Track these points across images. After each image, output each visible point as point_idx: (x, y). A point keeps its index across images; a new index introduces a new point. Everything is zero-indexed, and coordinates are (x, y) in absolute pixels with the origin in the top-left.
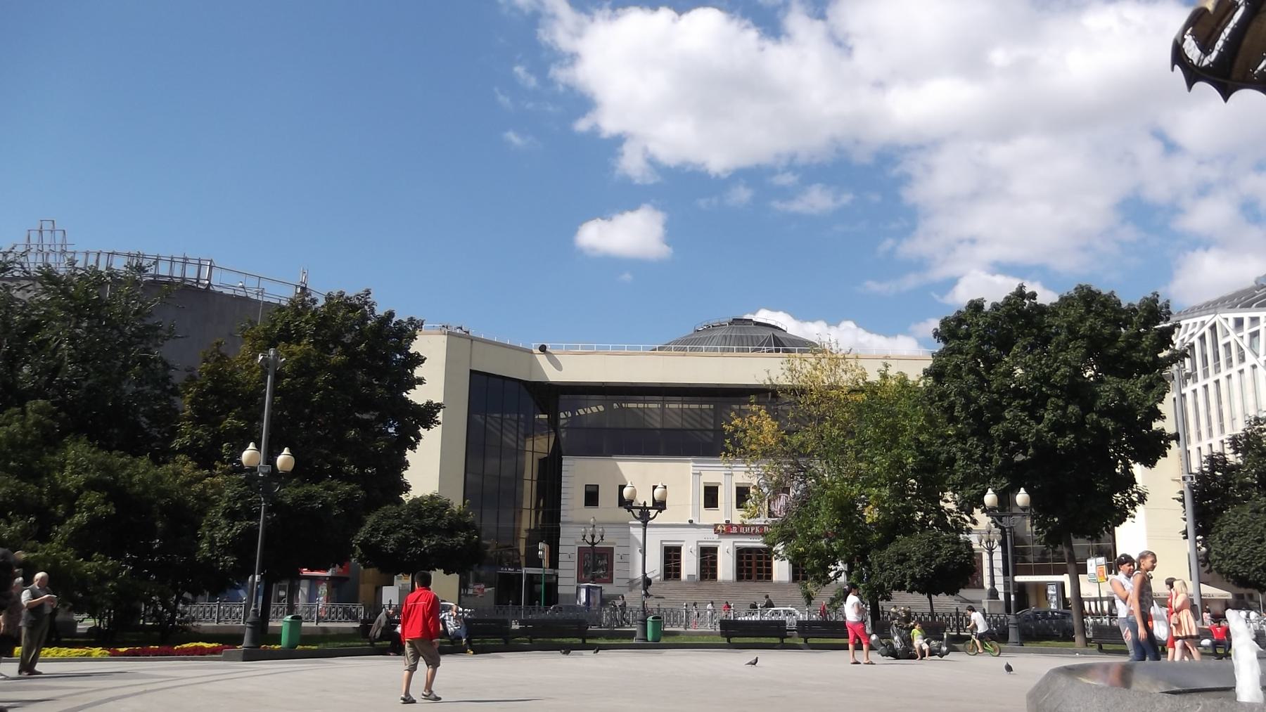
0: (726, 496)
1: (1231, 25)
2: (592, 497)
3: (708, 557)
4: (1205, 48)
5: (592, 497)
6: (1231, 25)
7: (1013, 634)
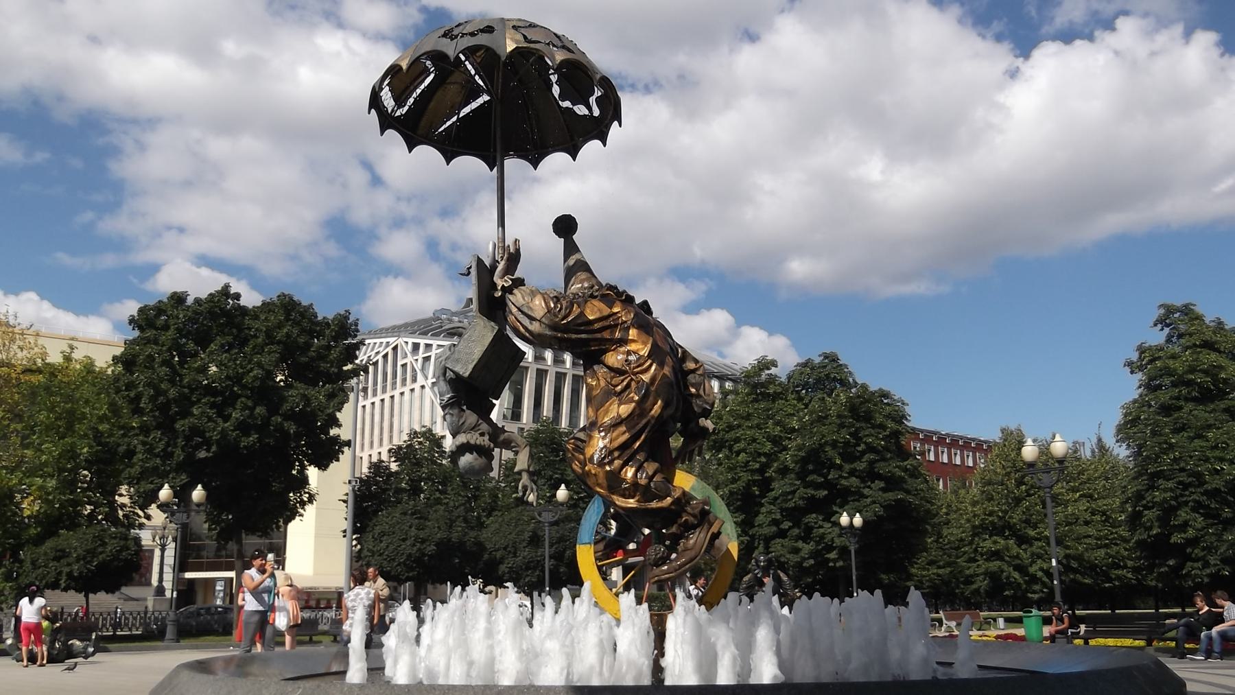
1: (422, 87)
4: (400, 102)
6: (422, 87)
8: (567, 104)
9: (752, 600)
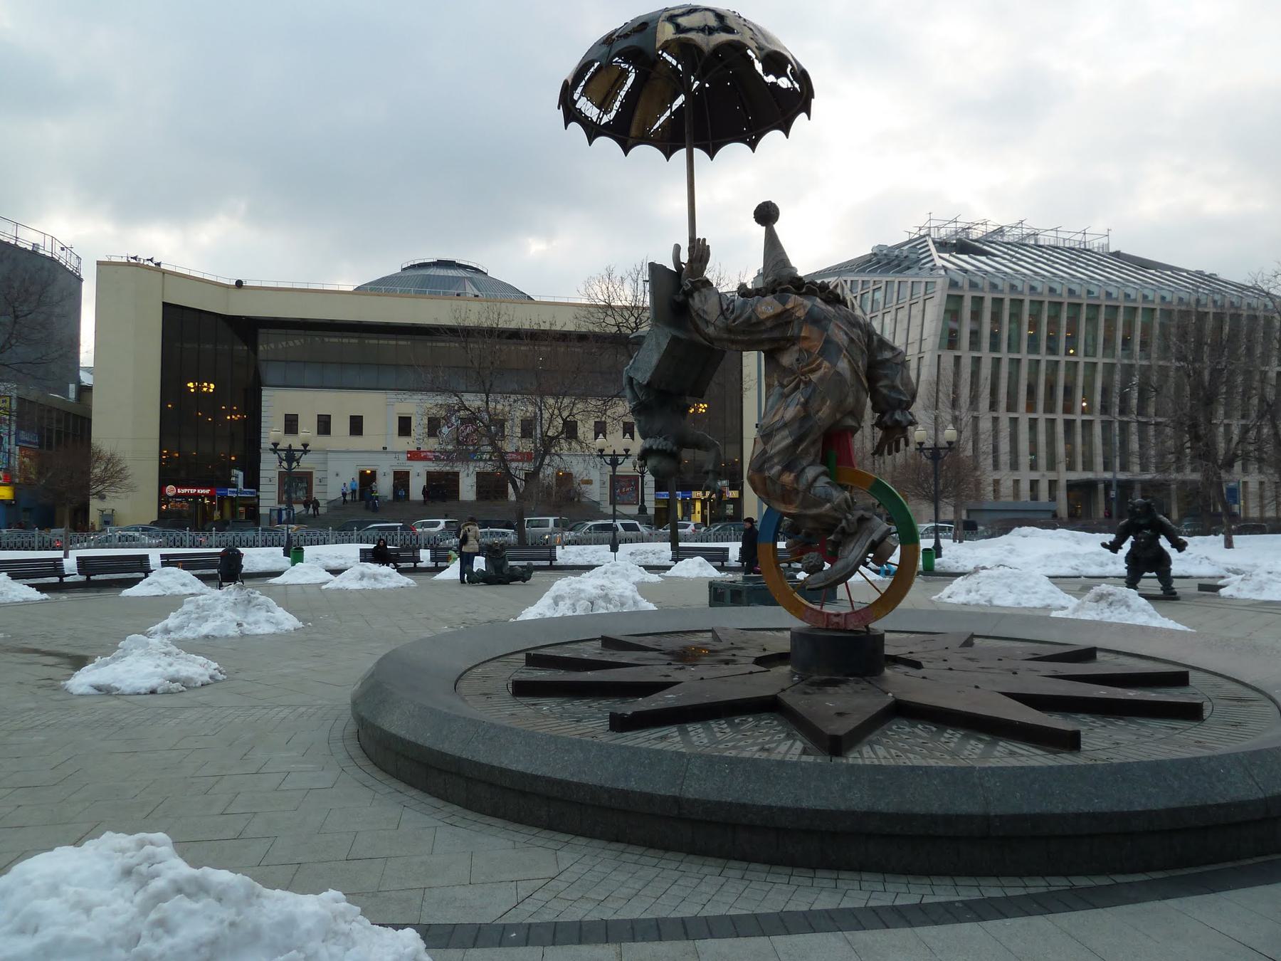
1: (626, 88)
2: (291, 424)
3: (401, 479)
4: (604, 106)
5: (291, 424)
6: (626, 88)
7: (975, 414)
8: (770, 79)
9: (367, 479)
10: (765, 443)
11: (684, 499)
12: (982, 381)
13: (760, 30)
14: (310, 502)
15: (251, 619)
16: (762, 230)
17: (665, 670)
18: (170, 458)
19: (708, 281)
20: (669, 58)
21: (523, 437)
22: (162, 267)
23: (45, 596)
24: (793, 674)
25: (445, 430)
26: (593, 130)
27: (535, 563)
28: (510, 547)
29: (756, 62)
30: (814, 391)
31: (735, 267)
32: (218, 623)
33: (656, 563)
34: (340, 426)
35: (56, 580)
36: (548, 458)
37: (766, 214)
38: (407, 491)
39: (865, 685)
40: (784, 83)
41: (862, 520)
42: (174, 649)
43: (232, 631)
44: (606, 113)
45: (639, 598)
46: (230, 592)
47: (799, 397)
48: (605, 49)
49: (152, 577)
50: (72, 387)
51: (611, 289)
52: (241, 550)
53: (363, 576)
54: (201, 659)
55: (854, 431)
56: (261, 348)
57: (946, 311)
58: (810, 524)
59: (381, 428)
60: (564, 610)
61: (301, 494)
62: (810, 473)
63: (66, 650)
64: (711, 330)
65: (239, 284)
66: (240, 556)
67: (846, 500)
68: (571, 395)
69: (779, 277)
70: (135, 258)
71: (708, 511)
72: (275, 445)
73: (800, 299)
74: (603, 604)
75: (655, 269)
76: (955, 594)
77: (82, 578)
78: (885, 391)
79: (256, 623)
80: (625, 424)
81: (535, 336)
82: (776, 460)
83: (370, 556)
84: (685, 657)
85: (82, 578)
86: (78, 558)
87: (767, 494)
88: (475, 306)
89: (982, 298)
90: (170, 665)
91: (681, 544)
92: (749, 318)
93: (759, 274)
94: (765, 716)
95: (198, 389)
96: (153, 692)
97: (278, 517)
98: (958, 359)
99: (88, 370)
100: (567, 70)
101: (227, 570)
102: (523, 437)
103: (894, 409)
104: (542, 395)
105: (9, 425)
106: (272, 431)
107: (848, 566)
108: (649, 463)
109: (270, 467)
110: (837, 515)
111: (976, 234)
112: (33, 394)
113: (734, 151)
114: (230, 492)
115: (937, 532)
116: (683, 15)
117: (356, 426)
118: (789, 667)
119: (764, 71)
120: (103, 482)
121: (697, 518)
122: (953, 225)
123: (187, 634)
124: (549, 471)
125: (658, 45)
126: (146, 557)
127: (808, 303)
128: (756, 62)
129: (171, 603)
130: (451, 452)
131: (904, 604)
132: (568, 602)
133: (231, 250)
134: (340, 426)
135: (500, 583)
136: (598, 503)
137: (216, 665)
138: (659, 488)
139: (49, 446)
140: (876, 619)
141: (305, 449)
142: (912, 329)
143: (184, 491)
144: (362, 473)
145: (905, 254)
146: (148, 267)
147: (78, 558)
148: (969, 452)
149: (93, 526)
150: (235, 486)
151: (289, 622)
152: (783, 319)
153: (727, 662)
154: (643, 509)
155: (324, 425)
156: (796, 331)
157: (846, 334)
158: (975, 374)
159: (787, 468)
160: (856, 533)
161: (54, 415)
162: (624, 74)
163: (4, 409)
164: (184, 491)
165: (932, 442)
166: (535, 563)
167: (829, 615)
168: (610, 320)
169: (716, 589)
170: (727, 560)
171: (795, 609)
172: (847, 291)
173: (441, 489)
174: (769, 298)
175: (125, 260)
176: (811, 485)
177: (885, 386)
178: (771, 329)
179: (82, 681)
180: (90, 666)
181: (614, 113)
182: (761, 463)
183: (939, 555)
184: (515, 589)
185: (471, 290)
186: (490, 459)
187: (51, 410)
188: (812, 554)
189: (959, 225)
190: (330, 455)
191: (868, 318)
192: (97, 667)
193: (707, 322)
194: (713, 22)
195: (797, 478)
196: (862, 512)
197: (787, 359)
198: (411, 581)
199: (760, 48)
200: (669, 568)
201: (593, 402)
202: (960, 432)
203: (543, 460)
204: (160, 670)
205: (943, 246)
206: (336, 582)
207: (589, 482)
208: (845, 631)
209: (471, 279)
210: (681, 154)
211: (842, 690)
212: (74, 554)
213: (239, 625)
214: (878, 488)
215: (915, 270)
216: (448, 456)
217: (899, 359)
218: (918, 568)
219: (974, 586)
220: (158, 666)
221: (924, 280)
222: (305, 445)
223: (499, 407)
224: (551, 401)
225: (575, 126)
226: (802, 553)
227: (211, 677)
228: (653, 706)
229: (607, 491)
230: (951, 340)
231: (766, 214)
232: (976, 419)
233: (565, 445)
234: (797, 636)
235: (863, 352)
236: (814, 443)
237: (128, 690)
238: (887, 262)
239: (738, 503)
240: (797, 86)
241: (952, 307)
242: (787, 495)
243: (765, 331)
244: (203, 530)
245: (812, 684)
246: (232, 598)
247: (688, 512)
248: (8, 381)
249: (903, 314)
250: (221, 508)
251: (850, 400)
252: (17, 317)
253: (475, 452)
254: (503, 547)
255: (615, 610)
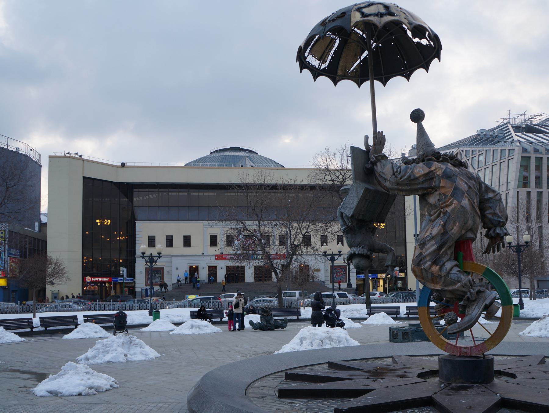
0: (221, 241)
1: (334, 49)
2: (152, 241)
3: (212, 271)
4: (322, 59)
5: (152, 241)
6: (334, 49)
8: (416, 40)
9: (194, 271)
10: (421, 249)
11: (373, 278)
12: (543, 205)
13: (410, 14)
14: (163, 285)
15: (132, 352)
16: (414, 126)
17: (366, 382)
18: (88, 262)
19: (385, 156)
20: (358, 31)
21: (280, 245)
22: (83, 157)
23: (23, 339)
24: (441, 383)
25: (236, 242)
26: (316, 73)
27: (288, 318)
28: (274, 308)
29: (408, 31)
30: (449, 218)
31: (400, 145)
32: (114, 354)
33: (358, 316)
34: (178, 241)
35: (29, 330)
36: (294, 257)
37: (417, 116)
38: (216, 278)
39: (483, 389)
40: (424, 42)
41: (479, 292)
42: (90, 370)
43: (122, 359)
44: (323, 63)
45: (349, 338)
46: (121, 337)
47: (440, 221)
48: (322, 28)
49: (79, 327)
50: (37, 224)
51: (328, 160)
52: (126, 312)
53: (192, 327)
54: (105, 376)
55: (473, 240)
56: (135, 199)
57: (521, 166)
58: (449, 296)
59: (200, 242)
60: (305, 347)
61: (158, 280)
62: (448, 265)
63: (34, 370)
64: (387, 184)
65: (123, 165)
66: (125, 316)
67: (470, 281)
68: (307, 221)
69: (425, 151)
70: (68, 153)
71: (387, 286)
72: (143, 253)
73: (439, 165)
74: (329, 342)
75: (354, 150)
76: (533, 331)
77: (43, 329)
78: (490, 216)
79: (135, 354)
80: (338, 236)
81: (285, 188)
82: (428, 259)
83: (195, 315)
84: (378, 373)
85: (43, 329)
86: (40, 318)
87: (423, 278)
88: (252, 172)
89: (541, 158)
90: (89, 379)
91: (372, 305)
92: (410, 176)
93: (413, 148)
94: (425, 408)
95: (102, 223)
96: (80, 394)
97: (146, 293)
98: (529, 193)
99: (45, 214)
100: (301, 42)
101: (119, 324)
102: (280, 245)
103: (495, 226)
104: (290, 221)
105: (5, 246)
106: (141, 246)
107: (472, 319)
108: (353, 262)
109: (141, 266)
110: (464, 289)
111: (535, 122)
112: (17, 228)
113: (397, 81)
114: (120, 280)
115: (520, 294)
116: (365, 7)
117: (187, 241)
118: (438, 379)
119: (412, 36)
120: (53, 276)
121: (381, 289)
122: (523, 117)
123: (98, 360)
124: (296, 264)
125: (352, 24)
126: (76, 317)
127: (443, 167)
128: (408, 31)
129: (88, 343)
130: (239, 255)
131: (505, 339)
132: (308, 341)
133: (123, 148)
134: (178, 241)
135: (269, 329)
136: (324, 282)
137: (113, 379)
138: (358, 273)
139: (25, 257)
140: (488, 350)
141: (159, 255)
142: (501, 177)
143: (95, 279)
144: (191, 268)
145: (496, 134)
146: (75, 158)
147: (40, 318)
148: (537, 248)
149: (48, 300)
150: (122, 276)
151: (152, 353)
152: (430, 176)
153: (402, 377)
154: (349, 285)
155: (170, 241)
156: (437, 183)
157: (466, 184)
158: (539, 201)
159: (435, 263)
160: (475, 300)
161: (28, 240)
162: (333, 41)
163: (2, 237)
164: (95, 279)
165: (516, 242)
166: (288, 318)
167: (461, 348)
168: (328, 178)
169: (393, 332)
170: (399, 314)
171: (440, 344)
172: (463, 156)
173: (235, 275)
174: (421, 164)
175: (63, 155)
176: (448, 273)
177: (490, 213)
178: (423, 182)
179: (42, 388)
180: (47, 380)
181: (328, 63)
182: (418, 261)
183: (522, 308)
184: (276, 334)
185: (249, 163)
186: (262, 259)
187: (26, 237)
188: (450, 313)
189: (526, 117)
190: (173, 258)
191: (476, 171)
192: (50, 380)
193: (385, 179)
194: (382, 10)
195: (440, 269)
196: (479, 288)
197: (433, 199)
198: (219, 329)
199: (410, 23)
200: (366, 319)
201: (320, 225)
202: (532, 236)
203: (292, 258)
204: (83, 382)
205: (517, 129)
206: (178, 330)
207: (318, 270)
208: (470, 357)
209: (249, 157)
210: (367, 84)
211: (470, 392)
212: (39, 315)
213: (126, 355)
214: (487, 273)
215: (502, 143)
216: (237, 257)
217: (497, 198)
218: (512, 315)
219: (544, 326)
220: (82, 380)
221: (507, 148)
222: (159, 254)
223: (266, 229)
224: (295, 225)
225: (306, 71)
226: (444, 312)
227: (111, 386)
228: (360, 404)
229: (329, 275)
230: (524, 182)
231: (417, 116)
232: (540, 227)
233: (304, 249)
234: (443, 361)
235: (477, 194)
236: (450, 248)
237: (67, 394)
238: (485, 139)
239: (404, 280)
240: (432, 43)
241: (525, 164)
242: (434, 279)
243: (419, 183)
244: (106, 301)
245: (452, 389)
246: (121, 341)
247: (375, 287)
248: (4, 222)
249: (496, 169)
250: (115, 288)
251: (470, 222)
252: (8, 188)
253: (253, 254)
254: (270, 309)
255: (335, 346)
